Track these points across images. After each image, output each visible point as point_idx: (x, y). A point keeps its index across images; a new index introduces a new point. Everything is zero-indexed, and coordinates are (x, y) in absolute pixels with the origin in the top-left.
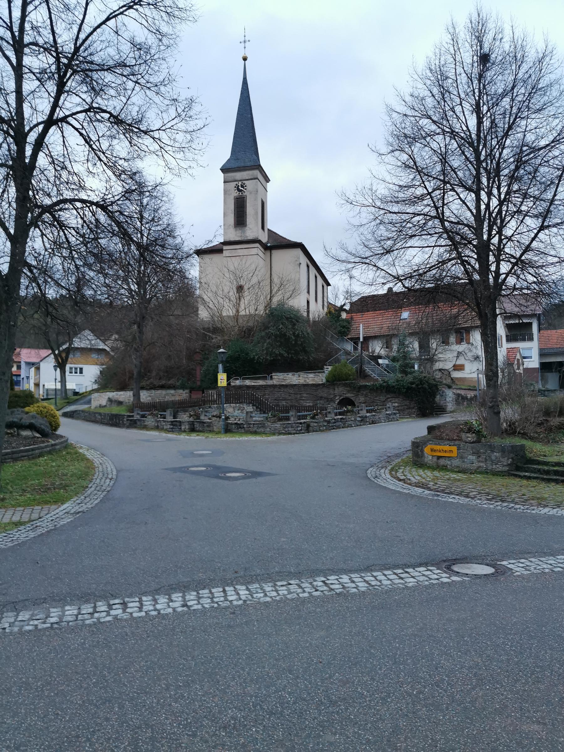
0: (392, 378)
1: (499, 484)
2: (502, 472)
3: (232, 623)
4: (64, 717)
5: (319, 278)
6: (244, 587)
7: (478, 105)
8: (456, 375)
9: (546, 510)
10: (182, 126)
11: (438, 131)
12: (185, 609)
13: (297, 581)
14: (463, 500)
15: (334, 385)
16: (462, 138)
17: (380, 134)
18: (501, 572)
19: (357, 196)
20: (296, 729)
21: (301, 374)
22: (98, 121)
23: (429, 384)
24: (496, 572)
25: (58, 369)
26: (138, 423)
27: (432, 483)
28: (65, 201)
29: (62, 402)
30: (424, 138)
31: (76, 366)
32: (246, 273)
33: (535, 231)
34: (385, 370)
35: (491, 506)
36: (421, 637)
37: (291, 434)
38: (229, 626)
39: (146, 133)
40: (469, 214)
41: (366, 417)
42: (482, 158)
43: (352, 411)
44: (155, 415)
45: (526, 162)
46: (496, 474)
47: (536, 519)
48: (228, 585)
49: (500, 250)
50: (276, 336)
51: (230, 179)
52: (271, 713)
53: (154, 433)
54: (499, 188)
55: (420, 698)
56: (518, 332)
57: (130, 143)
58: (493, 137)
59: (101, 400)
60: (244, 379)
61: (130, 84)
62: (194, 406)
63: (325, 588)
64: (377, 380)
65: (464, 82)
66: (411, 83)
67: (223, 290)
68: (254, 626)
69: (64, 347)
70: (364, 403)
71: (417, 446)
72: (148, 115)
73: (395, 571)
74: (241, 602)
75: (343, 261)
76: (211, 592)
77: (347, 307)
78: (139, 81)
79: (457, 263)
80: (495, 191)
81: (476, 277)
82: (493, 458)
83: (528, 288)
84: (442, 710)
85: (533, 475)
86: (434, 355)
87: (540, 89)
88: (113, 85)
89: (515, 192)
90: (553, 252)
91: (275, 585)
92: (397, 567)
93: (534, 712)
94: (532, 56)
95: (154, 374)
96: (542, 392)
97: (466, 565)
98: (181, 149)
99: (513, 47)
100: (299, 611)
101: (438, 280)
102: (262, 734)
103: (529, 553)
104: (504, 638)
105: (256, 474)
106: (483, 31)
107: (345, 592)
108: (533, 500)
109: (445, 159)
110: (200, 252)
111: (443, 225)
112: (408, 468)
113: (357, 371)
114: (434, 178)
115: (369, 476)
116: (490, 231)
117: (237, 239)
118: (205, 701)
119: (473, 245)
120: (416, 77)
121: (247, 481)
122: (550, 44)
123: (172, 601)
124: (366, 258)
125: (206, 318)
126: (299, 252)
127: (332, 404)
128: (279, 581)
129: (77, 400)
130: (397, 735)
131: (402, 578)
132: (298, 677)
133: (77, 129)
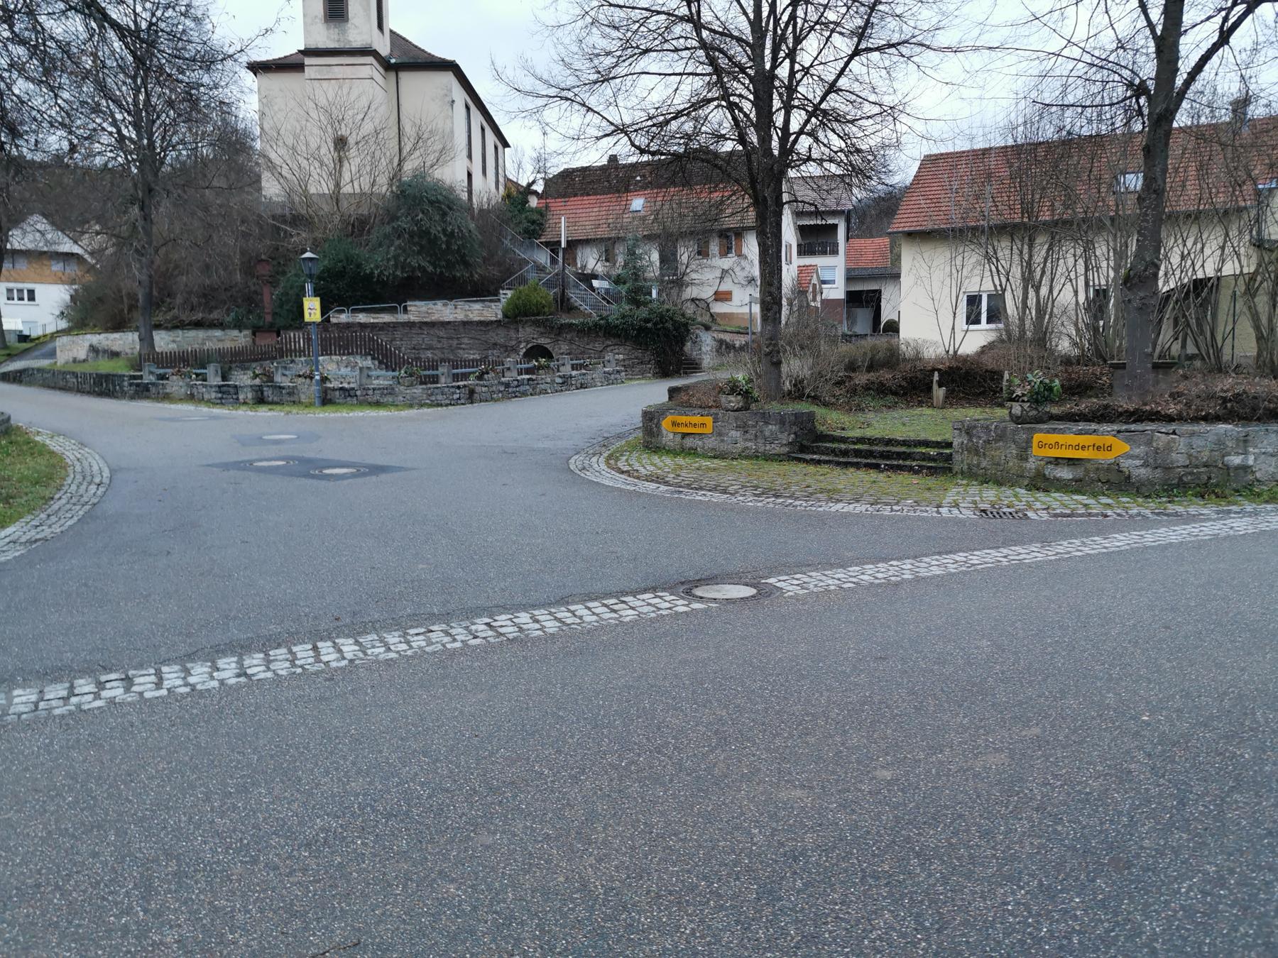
0: (614, 312)
1: (774, 473)
2: (779, 455)
3: (328, 694)
4: (13, 861)
6: (351, 641)
8: (718, 308)
9: (839, 506)
12: (243, 679)
13: (444, 627)
14: (717, 497)
18: (765, 593)
20: (431, 834)
21: (460, 303)
24: (759, 593)
26: (153, 390)
31: (20, 286)
32: (350, 113)
34: (604, 299)
37: (441, 405)
46: (769, 458)
47: (822, 519)
49: (791, 89)
52: (389, 816)
56: (816, 238)
59: (75, 349)
60: (354, 311)
63: (490, 633)
67: (307, 145)
68: (367, 694)
71: (651, 418)
74: (344, 663)
76: (290, 652)
77: (539, 187)
82: (767, 434)
85: (823, 458)
90: (872, 98)
92: (609, 595)
95: (179, 300)
96: (847, 338)
110: (257, 68)
111: (699, 34)
112: (635, 454)
117: (332, 45)
123: (218, 670)
125: (278, 196)
126: (449, 78)
128: (412, 627)
129: (26, 351)
131: (615, 611)
132: (438, 760)
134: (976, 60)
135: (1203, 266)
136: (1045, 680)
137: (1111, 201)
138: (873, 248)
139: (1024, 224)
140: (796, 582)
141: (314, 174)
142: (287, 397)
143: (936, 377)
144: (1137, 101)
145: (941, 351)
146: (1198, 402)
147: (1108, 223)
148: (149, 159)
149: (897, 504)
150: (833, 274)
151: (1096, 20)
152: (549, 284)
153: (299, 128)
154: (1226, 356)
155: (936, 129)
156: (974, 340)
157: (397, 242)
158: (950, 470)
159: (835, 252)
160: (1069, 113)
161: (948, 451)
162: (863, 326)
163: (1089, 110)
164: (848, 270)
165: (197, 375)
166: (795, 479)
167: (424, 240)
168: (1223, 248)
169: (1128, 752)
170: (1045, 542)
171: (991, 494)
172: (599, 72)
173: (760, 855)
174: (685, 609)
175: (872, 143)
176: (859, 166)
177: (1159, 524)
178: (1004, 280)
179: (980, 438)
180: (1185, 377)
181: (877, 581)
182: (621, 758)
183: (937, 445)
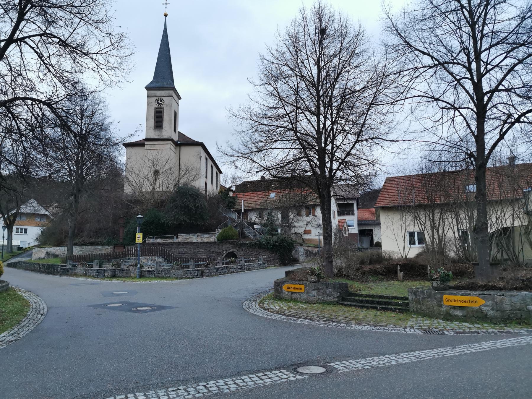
0: (263, 238)
2: (333, 302)
6: (142, 394)
7: (318, 60)
8: (306, 237)
9: (361, 327)
10: (115, 52)
13: (185, 387)
14: (307, 322)
15: (223, 243)
16: (308, 81)
17: (256, 74)
18: (330, 371)
21: (200, 235)
22: (50, 43)
23: (288, 243)
24: (327, 371)
25: (6, 229)
26: (70, 271)
28: (19, 98)
29: (8, 255)
30: (285, 78)
31: (22, 227)
32: (161, 161)
35: (326, 326)
37: (190, 278)
39: (86, 54)
41: (244, 265)
42: (321, 94)
43: (235, 261)
44: (84, 265)
47: (353, 333)
48: (129, 393)
49: (332, 154)
51: (152, 95)
53: (83, 279)
54: (331, 115)
56: (345, 209)
57: (74, 61)
60: (156, 238)
61: (77, 20)
63: (206, 391)
64: (253, 240)
66: (276, 43)
67: (143, 173)
69: (13, 212)
71: (278, 285)
72: (89, 43)
73: (258, 375)
77: (234, 189)
78: (84, 18)
80: (329, 116)
82: (328, 292)
83: (350, 180)
85: (353, 303)
86: (292, 223)
88: (63, 19)
90: (364, 158)
91: (167, 390)
92: (259, 371)
94: (351, 33)
96: (360, 249)
97: (307, 367)
98: (113, 68)
103: (349, 357)
105: (161, 308)
107: (220, 392)
110: (127, 145)
111: (296, 135)
112: (271, 301)
113: (239, 233)
115: (244, 307)
117: (156, 137)
119: (315, 149)
120: (279, 39)
121: (152, 313)
122: (362, 27)
125: (130, 192)
126: (200, 149)
127: (221, 256)
128: (170, 387)
129: (20, 254)
131: (262, 380)
133: (33, 48)
134: (404, 145)
135: (506, 222)
137: (464, 196)
138: (369, 213)
139: (429, 205)
141: (145, 184)
142: (125, 275)
143: (399, 267)
144: (470, 159)
145: (400, 256)
146: (511, 281)
147: (464, 205)
148: (80, 178)
149: (386, 326)
150: (352, 225)
151: (450, 130)
152: (236, 227)
154: (521, 259)
155: (390, 170)
156: (413, 251)
157: (175, 210)
158: (408, 310)
160: (443, 164)
161: (407, 302)
162: (366, 244)
163: (451, 163)
164: (359, 221)
165: (89, 265)
168: (513, 215)
170: (453, 346)
171: (427, 322)
172: (257, 148)
175: (365, 174)
176: (361, 182)
177: (502, 338)
179: (420, 296)
180: (505, 270)
181: (380, 366)
183: (401, 298)
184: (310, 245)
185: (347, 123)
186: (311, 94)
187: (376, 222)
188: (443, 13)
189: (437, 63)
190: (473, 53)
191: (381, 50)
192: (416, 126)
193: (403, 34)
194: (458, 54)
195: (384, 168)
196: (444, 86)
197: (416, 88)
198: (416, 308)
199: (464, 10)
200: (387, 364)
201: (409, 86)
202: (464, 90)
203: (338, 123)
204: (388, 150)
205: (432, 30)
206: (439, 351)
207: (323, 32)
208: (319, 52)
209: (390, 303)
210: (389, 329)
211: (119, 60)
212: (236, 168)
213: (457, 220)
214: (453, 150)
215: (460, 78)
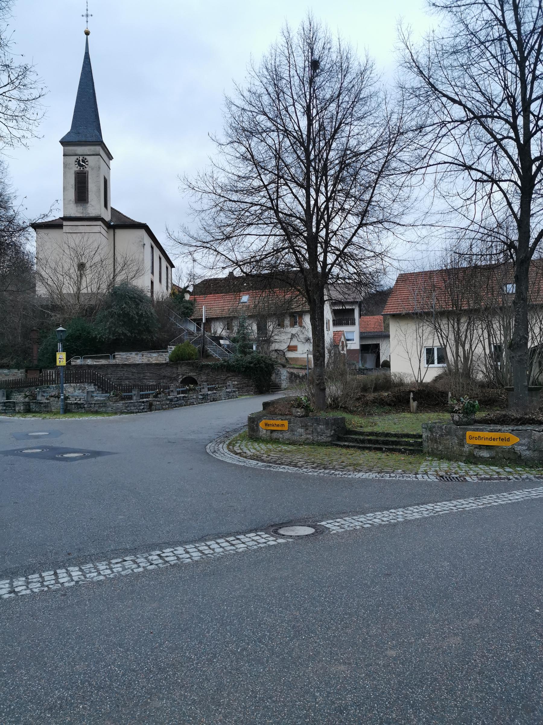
0: (232, 358)
1: (322, 454)
2: (326, 442)
5: (163, 260)
6: (77, 568)
7: (308, 107)
8: (290, 355)
9: (360, 474)
10: (15, 93)
11: (273, 128)
12: (12, 595)
13: (133, 557)
14: (291, 470)
16: (294, 137)
17: (220, 125)
18: (320, 531)
19: (199, 182)
21: (145, 353)
27: (266, 456)
30: (261, 134)
33: (356, 228)
34: (226, 350)
35: (315, 474)
36: (247, 598)
37: (133, 413)
38: (60, 608)
40: (300, 208)
41: (208, 395)
42: (312, 157)
43: (194, 389)
45: (349, 164)
46: (321, 444)
47: (351, 483)
48: (59, 568)
49: (327, 242)
50: (119, 315)
51: (71, 153)
52: (99, 688)
54: (326, 187)
55: (243, 655)
56: (343, 317)
58: (322, 139)
60: (85, 358)
62: (30, 386)
63: (160, 561)
64: (218, 360)
65: (296, 84)
67: (63, 267)
68: (86, 605)
70: (205, 382)
71: (253, 421)
73: (227, 539)
74: (73, 583)
75: (185, 245)
76: (41, 576)
77: (191, 289)
79: (289, 252)
80: (323, 189)
81: (307, 266)
82: (319, 430)
84: (262, 664)
85: (351, 444)
86: (271, 336)
87: (361, 99)
89: (339, 191)
90: (369, 248)
91: (110, 563)
92: (230, 535)
93: (341, 654)
94: (355, 68)
96: (361, 371)
97: (291, 528)
98: (14, 117)
99: (339, 57)
100: (133, 586)
101: (274, 267)
102: (90, 710)
103: (344, 513)
104: (319, 591)
105: (97, 454)
106: (314, 39)
107: (179, 563)
108: (350, 466)
109: (279, 154)
110: (36, 226)
111: (277, 216)
112: (244, 442)
113: (199, 351)
114: (270, 172)
115: (208, 451)
116: (318, 224)
117: (79, 215)
118: (30, 685)
120: (253, 74)
122: (370, 59)
124: (207, 243)
126: (143, 232)
127: (175, 382)
130: (221, 692)
131: (233, 545)
136: (480, 587)
138: (374, 322)
140: (337, 524)
141: (66, 283)
142: (43, 409)
143: (412, 395)
145: (413, 379)
147: (499, 311)
149: (393, 472)
150: (352, 336)
152: (196, 342)
153: (58, 259)
156: (431, 373)
158: (422, 451)
159: (353, 324)
161: (420, 440)
162: (370, 364)
164: (361, 333)
166: (335, 457)
167: (126, 319)
169: (528, 634)
171: (445, 465)
173: (320, 711)
174: (274, 543)
178: (445, 341)
179: (437, 433)
181: (383, 523)
182: (237, 646)
183: (413, 436)
184: (296, 367)
185: (348, 199)
186: (298, 157)
187: (384, 334)
188: (482, 43)
189: (472, 116)
190: (521, 103)
191: (396, 94)
192: (441, 205)
193: (426, 73)
194: (500, 105)
195: (395, 264)
196: (479, 148)
197: (441, 151)
198: (432, 448)
199: (511, 39)
200: (392, 521)
201: (433, 148)
202: (505, 155)
203: (335, 200)
204: (402, 237)
205: (465, 68)
206: (458, 504)
207: (315, 65)
208: (310, 94)
209: (399, 442)
210: (396, 476)
211: (22, 105)
212: (194, 261)
213: (488, 332)
214: (489, 239)
215: (501, 137)
